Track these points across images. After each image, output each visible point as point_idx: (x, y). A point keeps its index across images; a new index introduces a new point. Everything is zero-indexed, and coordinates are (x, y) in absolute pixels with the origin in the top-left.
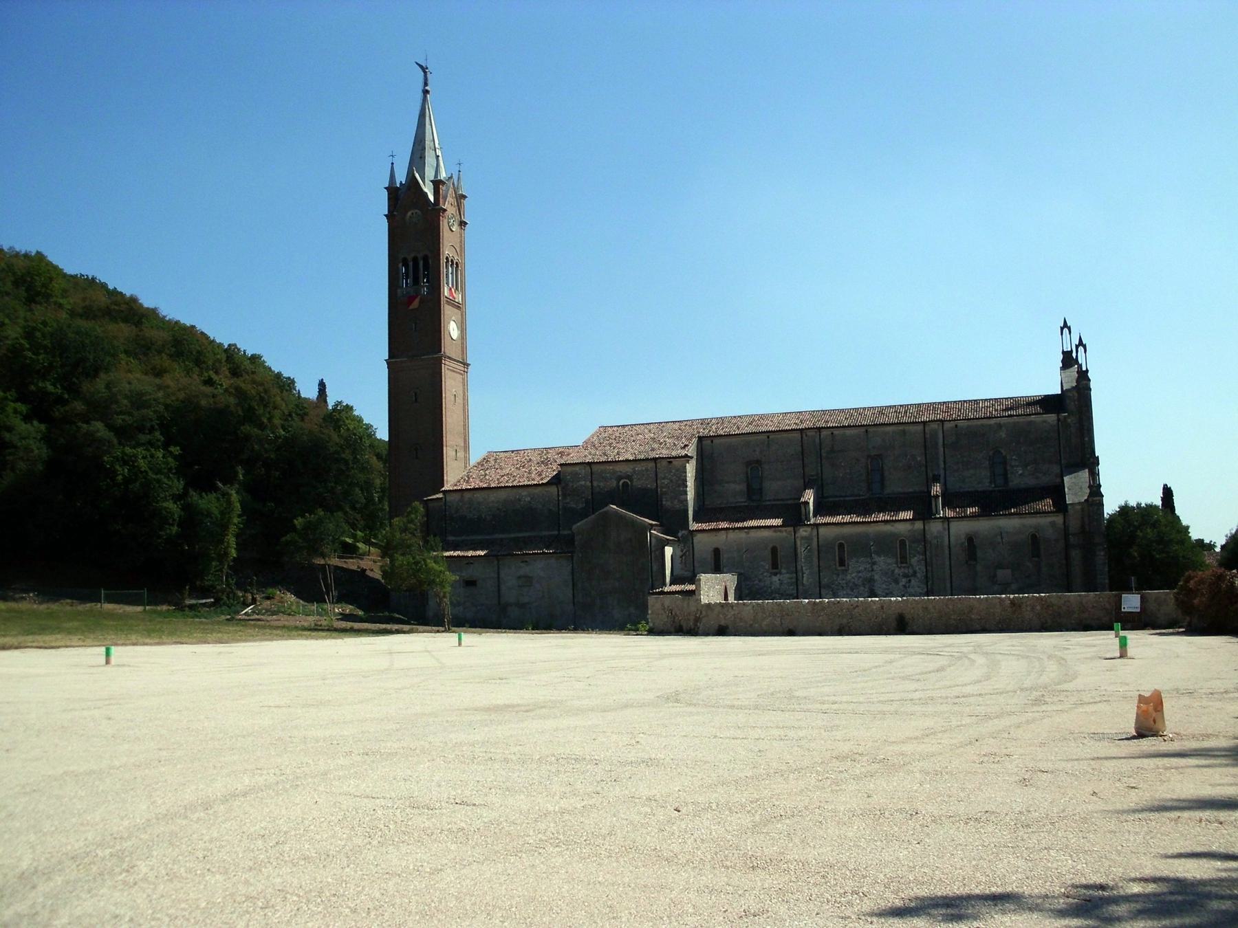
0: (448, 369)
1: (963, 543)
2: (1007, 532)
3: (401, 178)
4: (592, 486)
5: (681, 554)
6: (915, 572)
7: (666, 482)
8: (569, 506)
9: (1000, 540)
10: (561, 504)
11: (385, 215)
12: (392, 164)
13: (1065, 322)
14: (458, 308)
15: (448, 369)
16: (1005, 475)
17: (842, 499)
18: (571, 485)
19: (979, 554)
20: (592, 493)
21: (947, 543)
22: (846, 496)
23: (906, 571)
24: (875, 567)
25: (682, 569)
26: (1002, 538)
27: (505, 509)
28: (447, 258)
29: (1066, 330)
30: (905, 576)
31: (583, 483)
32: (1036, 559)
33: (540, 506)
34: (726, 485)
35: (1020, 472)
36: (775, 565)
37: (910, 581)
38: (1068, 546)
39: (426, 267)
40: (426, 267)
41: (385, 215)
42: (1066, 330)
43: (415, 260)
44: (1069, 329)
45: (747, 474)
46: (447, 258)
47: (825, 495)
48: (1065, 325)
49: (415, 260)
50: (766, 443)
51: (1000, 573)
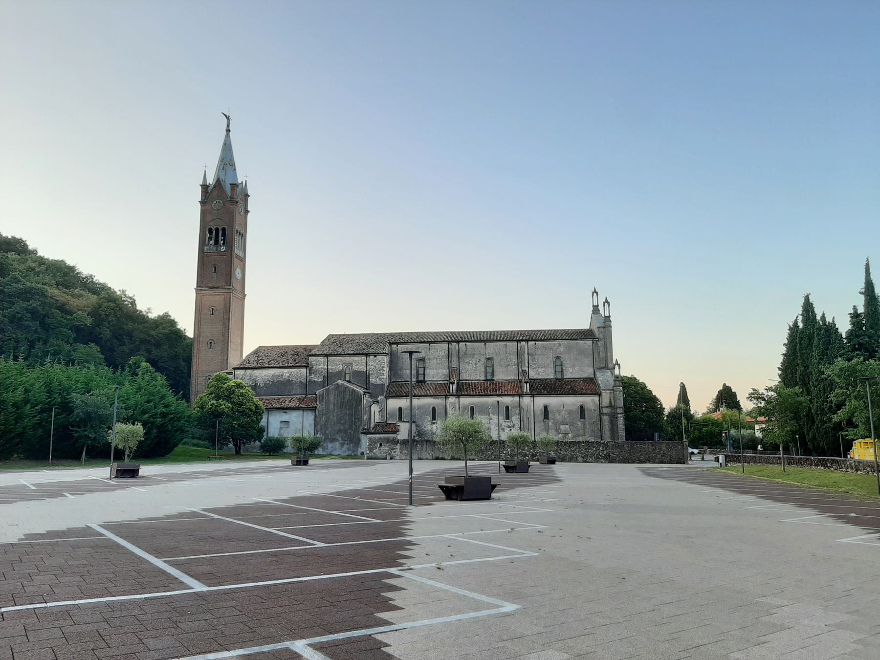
0: (234, 296)
1: (541, 409)
2: (566, 404)
3: (211, 180)
4: (328, 368)
5: (380, 410)
6: (514, 425)
7: (372, 367)
8: (313, 379)
9: (563, 409)
10: (308, 378)
11: (199, 202)
12: (205, 171)
13: (606, 299)
14: (242, 261)
15: (234, 296)
16: (562, 372)
17: (471, 381)
18: (314, 366)
19: (550, 416)
20: (327, 373)
21: (533, 409)
22: (472, 380)
23: (509, 424)
24: (491, 421)
25: (379, 419)
26: (564, 408)
27: (272, 380)
28: (237, 231)
29: (606, 304)
30: (509, 427)
31: (322, 366)
32: (583, 420)
33: (295, 379)
34: (404, 371)
35: (571, 371)
36: (434, 418)
37: (511, 430)
38: (601, 414)
39: (224, 234)
40: (224, 234)
41: (199, 202)
42: (606, 304)
43: (217, 230)
44: (608, 303)
45: (417, 365)
46: (237, 231)
47: (460, 379)
48: (595, 292)
49: (217, 230)
50: (428, 348)
51: (562, 427)
